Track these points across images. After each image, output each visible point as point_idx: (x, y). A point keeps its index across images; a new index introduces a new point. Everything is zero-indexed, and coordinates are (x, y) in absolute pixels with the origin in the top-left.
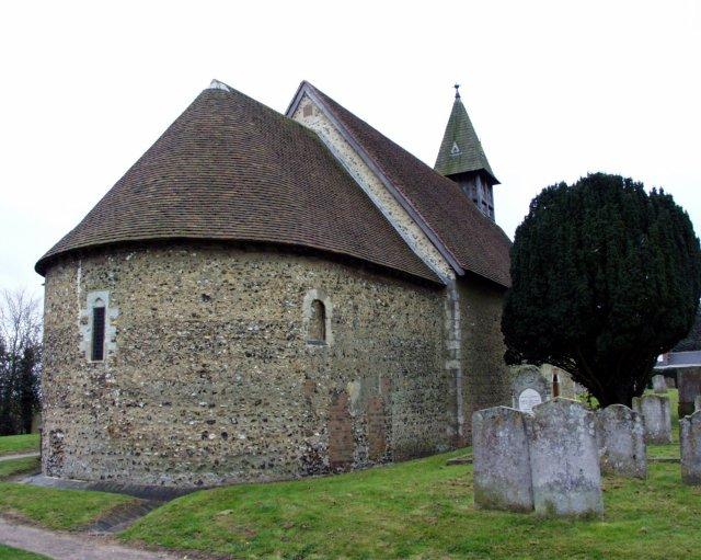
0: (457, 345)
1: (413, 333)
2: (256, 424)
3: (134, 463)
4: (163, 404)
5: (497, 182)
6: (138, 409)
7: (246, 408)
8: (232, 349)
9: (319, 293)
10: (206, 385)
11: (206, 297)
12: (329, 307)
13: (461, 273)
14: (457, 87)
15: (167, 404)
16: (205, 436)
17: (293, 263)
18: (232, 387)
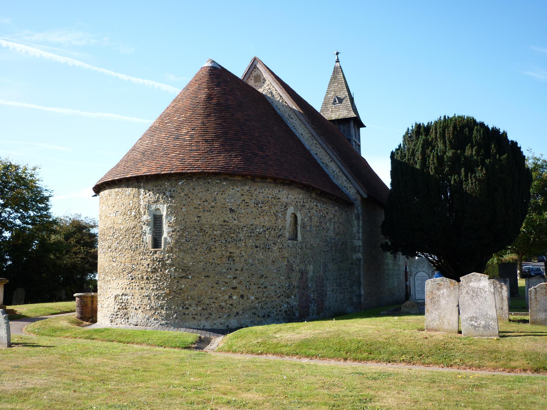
0: (360, 243)
1: (337, 234)
2: (260, 290)
3: (184, 314)
4: (205, 277)
5: (363, 126)
6: (187, 280)
7: (254, 280)
8: (247, 242)
9: (295, 209)
10: (232, 265)
11: (232, 210)
12: (298, 215)
13: (365, 196)
14: (337, 54)
15: (207, 276)
16: (230, 297)
17: (281, 190)
18: (246, 267)
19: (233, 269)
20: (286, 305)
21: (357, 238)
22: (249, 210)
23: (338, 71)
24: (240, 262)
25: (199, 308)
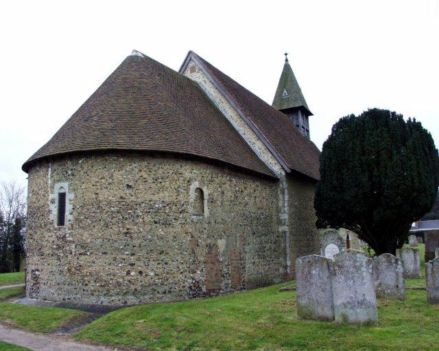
0: (286, 216)
1: (259, 209)
2: (160, 266)
3: (84, 290)
4: (102, 253)
5: (311, 114)
6: (86, 256)
7: (154, 256)
8: (146, 218)
9: (200, 184)
10: (129, 241)
11: (129, 186)
12: (206, 192)
13: (289, 171)
14: (286, 54)
15: (105, 253)
16: (128, 273)
17: (183, 165)
18: (145, 243)
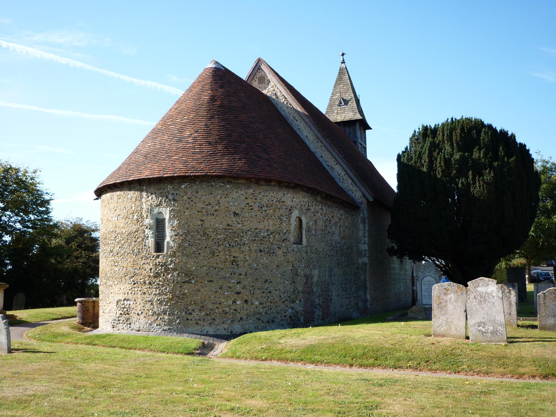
0: (366, 247)
1: (343, 238)
2: (265, 295)
3: (187, 319)
4: (208, 281)
5: (369, 128)
6: (190, 285)
7: (258, 284)
8: (251, 246)
9: (299, 213)
10: (236, 270)
11: (235, 214)
12: (303, 219)
13: (371, 199)
14: (343, 55)
15: (211, 281)
16: (234, 302)
17: (285, 193)
18: (250, 272)
19: (237, 274)
20: (290, 311)
21: (362, 242)
22: (253, 214)
23: (343, 72)
24: (244, 267)
25: (203, 314)
